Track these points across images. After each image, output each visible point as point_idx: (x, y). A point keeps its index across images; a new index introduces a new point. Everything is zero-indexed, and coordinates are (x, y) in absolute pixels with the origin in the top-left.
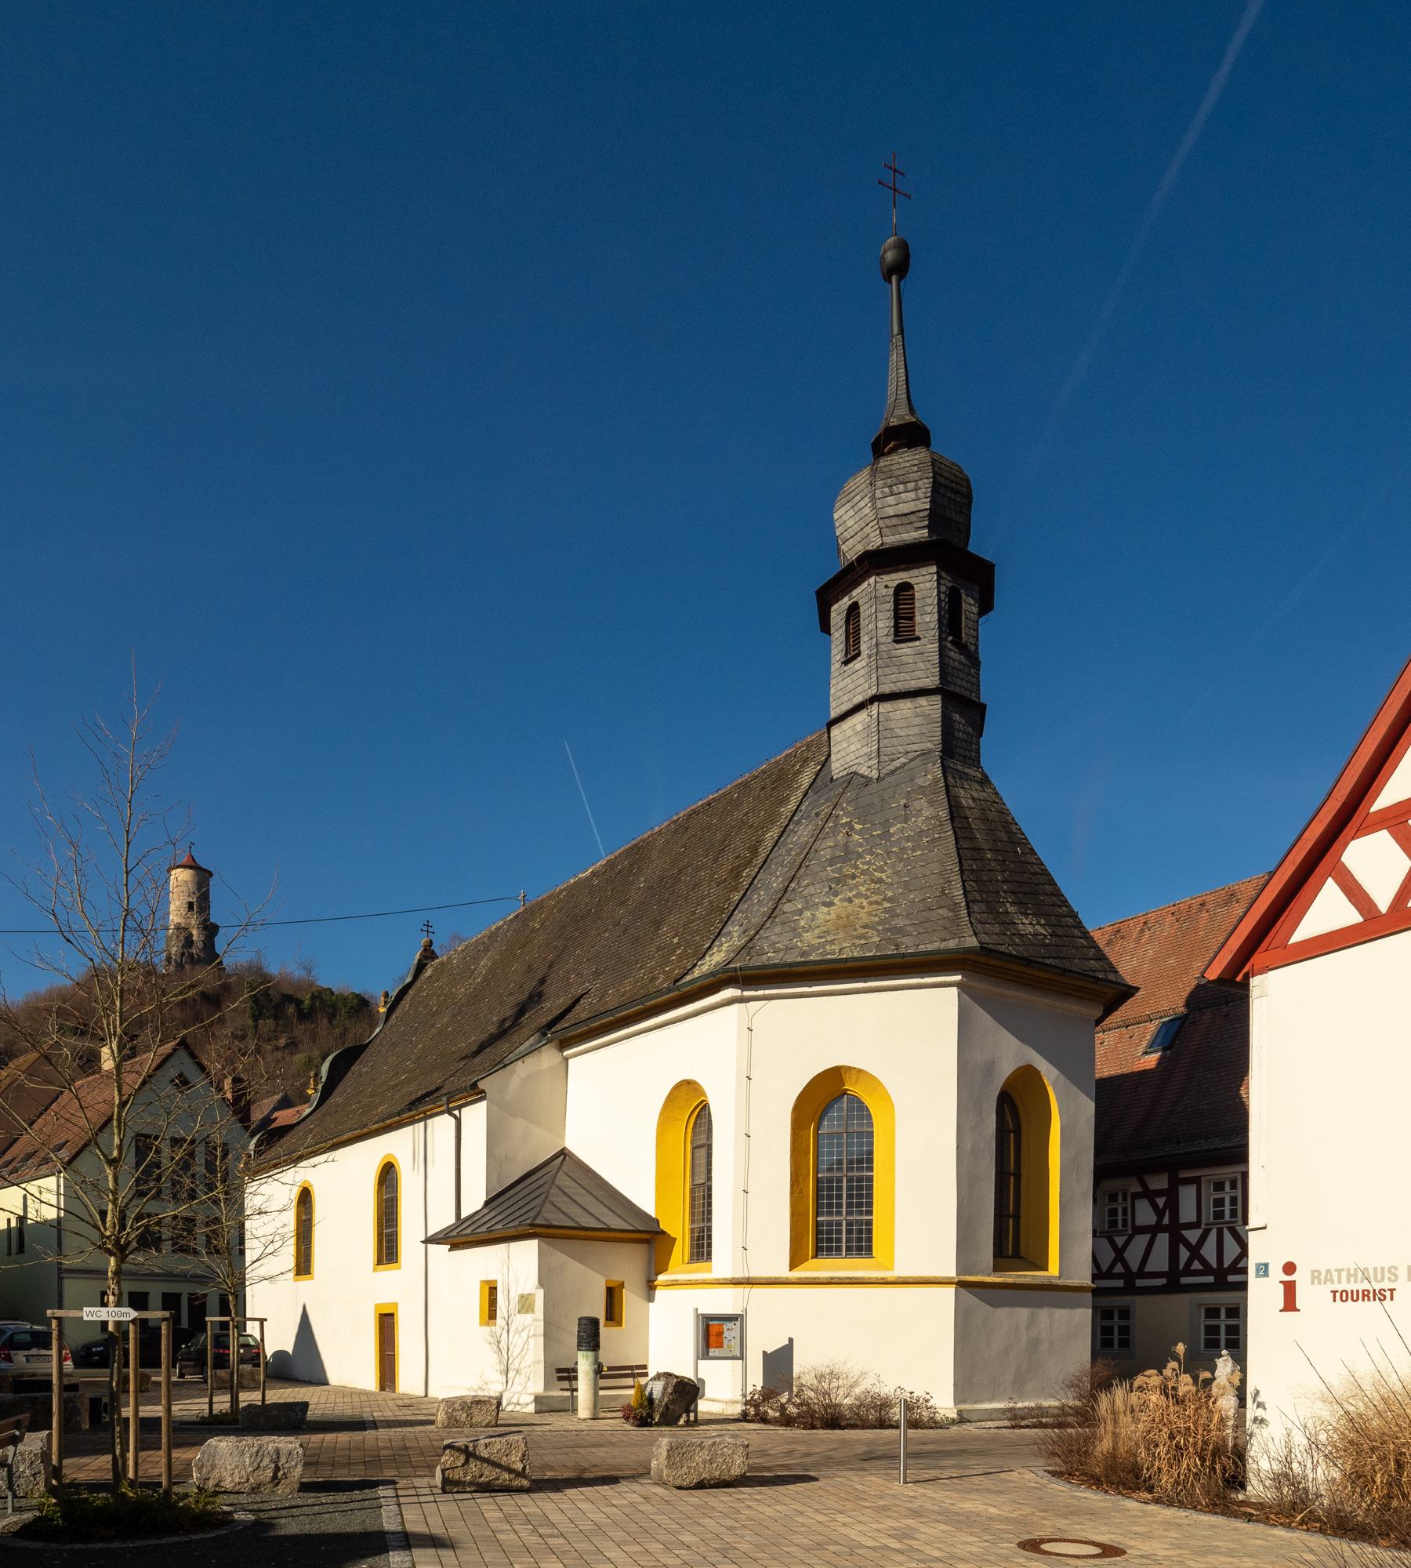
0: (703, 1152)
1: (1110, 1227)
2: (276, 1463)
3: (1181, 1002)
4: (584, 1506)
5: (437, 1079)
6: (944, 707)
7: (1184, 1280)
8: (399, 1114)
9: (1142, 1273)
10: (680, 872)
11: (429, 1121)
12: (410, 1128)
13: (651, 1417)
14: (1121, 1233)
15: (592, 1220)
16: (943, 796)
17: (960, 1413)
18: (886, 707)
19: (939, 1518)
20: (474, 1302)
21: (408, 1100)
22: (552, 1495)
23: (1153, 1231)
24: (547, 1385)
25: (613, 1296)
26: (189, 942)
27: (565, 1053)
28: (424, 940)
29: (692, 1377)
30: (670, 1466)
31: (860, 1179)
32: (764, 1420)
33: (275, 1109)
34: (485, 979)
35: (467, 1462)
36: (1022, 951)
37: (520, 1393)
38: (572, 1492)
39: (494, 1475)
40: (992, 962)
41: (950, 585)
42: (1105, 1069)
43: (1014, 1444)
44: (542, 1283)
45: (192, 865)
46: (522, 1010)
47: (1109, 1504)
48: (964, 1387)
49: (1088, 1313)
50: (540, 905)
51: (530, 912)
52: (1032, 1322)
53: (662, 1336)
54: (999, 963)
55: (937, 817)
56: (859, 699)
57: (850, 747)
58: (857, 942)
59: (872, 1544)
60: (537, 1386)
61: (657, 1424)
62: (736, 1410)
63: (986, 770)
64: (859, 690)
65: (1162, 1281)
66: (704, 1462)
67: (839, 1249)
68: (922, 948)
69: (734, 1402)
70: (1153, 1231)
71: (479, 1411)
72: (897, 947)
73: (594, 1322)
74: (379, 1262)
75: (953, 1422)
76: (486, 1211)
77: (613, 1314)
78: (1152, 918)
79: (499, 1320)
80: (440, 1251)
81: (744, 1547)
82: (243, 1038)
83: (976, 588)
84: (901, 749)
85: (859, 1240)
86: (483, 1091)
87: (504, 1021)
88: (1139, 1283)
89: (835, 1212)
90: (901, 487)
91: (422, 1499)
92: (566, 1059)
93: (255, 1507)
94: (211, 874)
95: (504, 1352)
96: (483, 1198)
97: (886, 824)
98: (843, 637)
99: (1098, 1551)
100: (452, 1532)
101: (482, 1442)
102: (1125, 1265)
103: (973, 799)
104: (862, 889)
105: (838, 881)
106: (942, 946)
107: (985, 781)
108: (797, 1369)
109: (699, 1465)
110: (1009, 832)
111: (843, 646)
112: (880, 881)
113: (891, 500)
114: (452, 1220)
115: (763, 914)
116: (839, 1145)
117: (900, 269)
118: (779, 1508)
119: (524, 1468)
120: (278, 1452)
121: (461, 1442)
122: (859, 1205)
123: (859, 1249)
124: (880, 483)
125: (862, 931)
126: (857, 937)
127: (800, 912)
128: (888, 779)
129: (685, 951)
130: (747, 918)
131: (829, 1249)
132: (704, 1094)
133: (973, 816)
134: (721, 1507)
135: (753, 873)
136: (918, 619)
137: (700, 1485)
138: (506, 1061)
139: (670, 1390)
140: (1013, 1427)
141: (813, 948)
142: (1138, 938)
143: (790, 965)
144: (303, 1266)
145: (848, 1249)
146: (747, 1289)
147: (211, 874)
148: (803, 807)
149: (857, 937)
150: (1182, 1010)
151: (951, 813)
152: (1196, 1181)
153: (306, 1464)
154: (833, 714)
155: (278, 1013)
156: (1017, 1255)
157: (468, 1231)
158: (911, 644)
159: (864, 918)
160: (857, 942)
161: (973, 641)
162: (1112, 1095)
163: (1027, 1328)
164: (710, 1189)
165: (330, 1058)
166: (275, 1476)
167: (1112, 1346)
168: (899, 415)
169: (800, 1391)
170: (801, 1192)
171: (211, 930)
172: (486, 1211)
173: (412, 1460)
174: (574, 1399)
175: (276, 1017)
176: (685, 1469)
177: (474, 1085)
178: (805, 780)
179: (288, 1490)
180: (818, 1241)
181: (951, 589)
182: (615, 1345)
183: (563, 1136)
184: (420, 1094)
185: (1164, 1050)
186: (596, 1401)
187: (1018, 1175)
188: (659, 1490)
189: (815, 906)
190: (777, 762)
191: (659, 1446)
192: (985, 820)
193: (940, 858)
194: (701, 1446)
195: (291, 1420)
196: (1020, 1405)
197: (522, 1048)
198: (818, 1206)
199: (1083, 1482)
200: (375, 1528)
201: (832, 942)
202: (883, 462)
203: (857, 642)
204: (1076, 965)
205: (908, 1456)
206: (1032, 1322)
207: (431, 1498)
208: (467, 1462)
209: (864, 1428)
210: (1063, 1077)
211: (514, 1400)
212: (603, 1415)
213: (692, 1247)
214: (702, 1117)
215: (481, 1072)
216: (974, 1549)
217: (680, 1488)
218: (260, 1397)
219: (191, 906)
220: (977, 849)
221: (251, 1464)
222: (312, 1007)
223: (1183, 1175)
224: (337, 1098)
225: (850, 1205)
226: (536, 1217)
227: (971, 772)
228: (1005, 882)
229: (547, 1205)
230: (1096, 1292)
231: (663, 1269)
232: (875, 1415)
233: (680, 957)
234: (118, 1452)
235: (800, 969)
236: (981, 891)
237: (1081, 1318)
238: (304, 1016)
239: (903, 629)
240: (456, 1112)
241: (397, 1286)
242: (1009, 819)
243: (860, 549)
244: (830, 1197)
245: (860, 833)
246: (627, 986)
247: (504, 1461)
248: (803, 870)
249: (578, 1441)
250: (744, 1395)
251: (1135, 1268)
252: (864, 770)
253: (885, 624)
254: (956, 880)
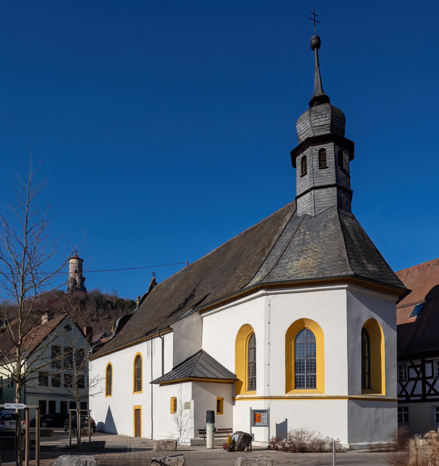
0: (253, 350)
1: (402, 379)
3: (424, 298)
5: (156, 325)
6: (338, 191)
7: (428, 397)
8: (142, 337)
10: (243, 251)
13: (234, 447)
15: (212, 375)
16: (338, 222)
17: (350, 446)
18: (317, 191)
21: (145, 332)
23: (416, 379)
24: (195, 436)
25: (219, 403)
26: (75, 283)
28: (153, 278)
32: (277, 449)
33: (101, 338)
36: (369, 276)
37: (186, 439)
40: (359, 280)
41: (338, 149)
42: (399, 322)
45: (77, 258)
46: (187, 301)
48: (351, 437)
49: (396, 410)
50: (193, 266)
51: (190, 268)
53: (238, 418)
54: (362, 281)
56: (307, 189)
57: (304, 205)
58: (309, 273)
62: (266, 445)
63: (353, 214)
64: (307, 185)
67: (304, 386)
68: (333, 275)
69: (265, 442)
70: (416, 379)
73: (213, 413)
75: (348, 450)
77: (220, 409)
79: (177, 412)
80: (156, 386)
84: (323, 206)
85: (311, 382)
86: (172, 329)
87: (180, 305)
88: (411, 398)
90: (320, 116)
92: (202, 318)
94: (83, 261)
96: (172, 367)
97: (318, 232)
98: (300, 168)
101: (167, 459)
102: (406, 392)
103: (349, 223)
105: (301, 252)
106: (341, 274)
107: (353, 217)
110: (363, 236)
111: (300, 171)
112: (316, 252)
113: (317, 121)
114: (161, 375)
117: (317, 46)
120: (86, 462)
121: (158, 459)
122: (311, 369)
124: (312, 115)
126: (308, 271)
127: (287, 263)
132: (253, 329)
136: (327, 161)
138: (180, 318)
139: (241, 438)
140: (371, 452)
142: (406, 277)
144: (109, 392)
145: (307, 386)
146: (269, 401)
147: (83, 261)
148: (287, 227)
149: (308, 271)
150: (424, 301)
151: (342, 227)
152: (432, 362)
154: (298, 194)
156: (369, 387)
159: (311, 265)
160: (309, 273)
164: (255, 364)
167: (402, 421)
168: (319, 93)
170: (289, 365)
171: (83, 279)
174: (205, 441)
175: (104, 308)
177: (169, 327)
178: (288, 218)
180: (296, 383)
181: (339, 151)
182: (221, 421)
184: (149, 330)
185: (418, 315)
187: (369, 358)
189: (293, 260)
191: (238, 461)
194: (254, 461)
195: (99, 448)
196: (373, 443)
201: (299, 273)
202: (313, 108)
204: (389, 281)
206: (375, 413)
210: (385, 323)
211: (183, 441)
212: (216, 447)
213: (249, 385)
214: (252, 337)
215: (171, 322)
218: (89, 439)
219: (76, 271)
222: (116, 305)
223: (426, 359)
224: (121, 333)
225: (307, 369)
226: (191, 374)
227: (348, 214)
229: (195, 369)
230: (399, 402)
231: (239, 393)
233: (243, 280)
234: (19, 462)
237: (394, 411)
238: (114, 308)
239: (322, 164)
240: (162, 336)
241: (141, 400)
245: (308, 235)
246: (224, 291)
248: (288, 248)
250: (269, 440)
251: (410, 393)
252: (309, 213)
253: (316, 163)
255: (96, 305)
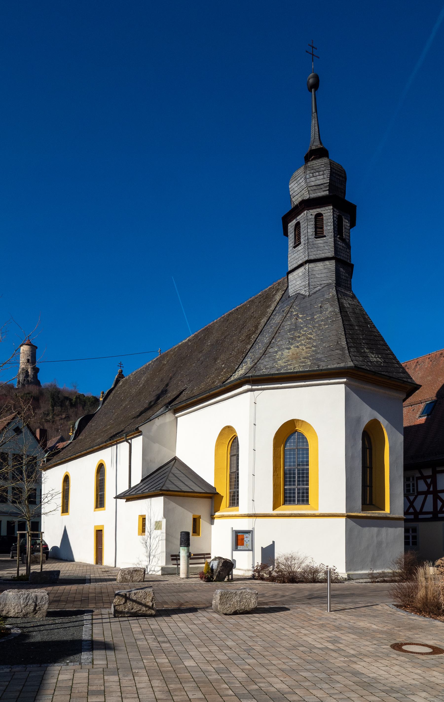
0: (235, 458)
2: (36, 603)
4: (180, 624)
5: (122, 427)
8: (105, 442)
9: (421, 512)
10: (225, 338)
11: (118, 445)
12: (110, 448)
13: (212, 577)
14: (412, 495)
16: (336, 302)
17: (348, 575)
18: (312, 265)
19: (350, 631)
20: (136, 524)
21: (110, 436)
22: (166, 618)
23: (426, 493)
25: (196, 522)
27: (177, 415)
29: (230, 558)
30: (220, 604)
31: (303, 470)
33: (57, 443)
34: (144, 385)
35: (126, 602)
37: (155, 566)
38: (175, 617)
39: (139, 608)
41: (338, 214)
43: (375, 590)
44: (165, 516)
47: (427, 623)
50: (167, 354)
51: (163, 357)
52: (378, 534)
53: (217, 541)
55: (334, 311)
56: (300, 262)
57: (297, 283)
58: (301, 364)
59: (319, 646)
60: (163, 563)
61: (215, 581)
62: (250, 574)
63: (354, 293)
65: (431, 516)
66: (237, 602)
67: (294, 501)
68: (329, 367)
69: (248, 570)
70: (426, 493)
71: (137, 575)
72: (319, 366)
73: (188, 534)
74: (97, 507)
76: (141, 484)
77: (196, 530)
78: (420, 360)
79: (147, 533)
80: (122, 502)
81: (258, 648)
82: (48, 414)
83: (349, 215)
84: (318, 283)
85: (303, 497)
86: (141, 432)
87: (151, 402)
88: (421, 516)
89: (292, 485)
90: (317, 173)
91: (104, 621)
92: (177, 418)
93: (23, 625)
94: (37, 348)
95: (148, 547)
97: (313, 315)
99: (430, 650)
100: (116, 640)
101: (133, 592)
103: (349, 304)
104: (303, 342)
105: (292, 339)
106: (338, 366)
107: (354, 297)
108: (276, 556)
109: (235, 603)
110: (364, 318)
111: (293, 240)
112: (310, 338)
113: (313, 179)
114: (127, 488)
115: (260, 354)
116: (294, 454)
117: (315, 86)
118: (273, 625)
119: (153, 605)
120: (36, 597)
121: (123, 592)
122: (303, 481)
123: (303, 501)
124: (308, 172)
125: (303, 360)
127: (276, 352)
128: (313, 296)
129: (227, 370)
130: (254, 355)
131: (290, 501)
133: (349, 311)
134: (245, 625)
135: (256, 337)
136: (325, 228)
137: (235, 613)
138: (151, 418)
139: (221, 565)
140: (372, 582)
141: (282, 367)
142: (415, 369)
143: (273, 374)
144: (65, 509)
145: (298, 501)
147: (37, 348)
148: (277, 309)
151: (340, 309)
153: (50, 604)
154: (289, 269)
155: (62, 404)
156: (371, 503)
157: (134, 493)
158: (322, 239)
159: (304, 355)
160: (301, 364)
161: (347, 237)
162: (409, 433)
163: (377, 536)
164: (238, 474)
165: (79, 420)
166: (35, 609)
168: (316, 145)
169: (278, 566)
170: (277, 475)
171: (36, 370)
172: (141, 484)
173: (102, 599)
174: (178, 569)
175: (61, 406)
176: (228, 605)
177: (137, 429)
178: (278, 297)
179: (41, 616)
180: (285, 497)
181: (338, 216)
183: (175, 451)
184: (115, 433)
185: (428, 415)
186: (188, 570)
187: (371, 468)
188: (216, 615)
189: (283, 349)
190: (266, 291)
191: (216, 594)
192: (354, 313)
193: (335, 330)
195: (52, 579)
197: (158, 413)
198: (285, 481)
199: (412, 611)
200: (78, 638)
201: (290, 365)
202: (309, 164)
203: (299, 238)
204: (395, 375)
205: (332, 596)
206: (378, 534)
207: (108, 620)
208: (126, 602)
209: (306, 582)
210: (390, 425)
211: (153, 569)
212: (191, 576)
213: (230, 500)
214: (235, 442)
216: (371, 649)
217: (226, 614)
218: (40, 568)
219: (28, 360)
220: (352, 325)
221: (23, 603)
222: (76, 401)
223: (438, 469)
225: (299, 481)
226: (162, 487)
227: (348, 293)
228: (363, 339)
229: (168, 481)
230: (406, 520)
231: (218, 510)
232: (311, 576)
233: (225, 372)
235: (276, 376)
236: (353, 343)
237: (398, 533)
238: (73, 405)
239: (319, 232)
240: (130, 441)
241: (104, 518)
242: (364, 313)
243: (300, 199)
244: (290, 478)
245: (302, 318)
246: (202, 386)
247: (143, 601)
248: (277, 334)
249: (180, 589)
250: (253, 567)
251: (418, 510)
252: (303, 292)
253: (311, 230)
254: (343, 338)
255: (52, 402)
